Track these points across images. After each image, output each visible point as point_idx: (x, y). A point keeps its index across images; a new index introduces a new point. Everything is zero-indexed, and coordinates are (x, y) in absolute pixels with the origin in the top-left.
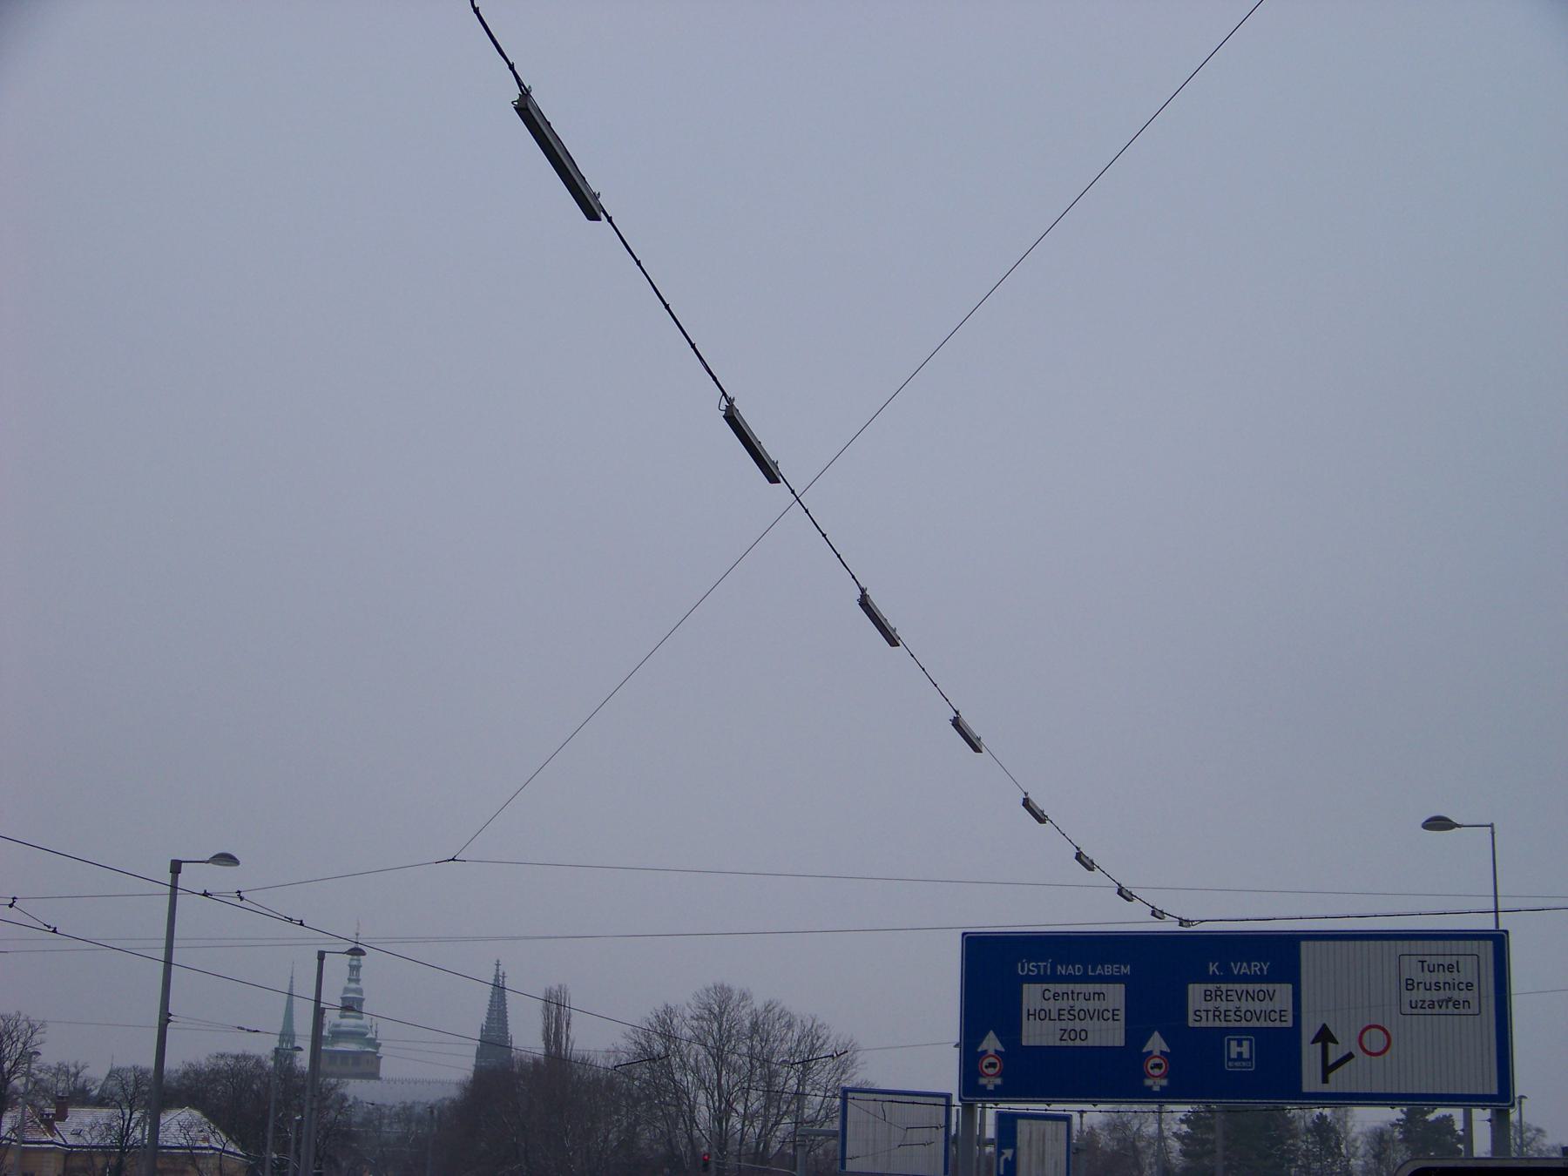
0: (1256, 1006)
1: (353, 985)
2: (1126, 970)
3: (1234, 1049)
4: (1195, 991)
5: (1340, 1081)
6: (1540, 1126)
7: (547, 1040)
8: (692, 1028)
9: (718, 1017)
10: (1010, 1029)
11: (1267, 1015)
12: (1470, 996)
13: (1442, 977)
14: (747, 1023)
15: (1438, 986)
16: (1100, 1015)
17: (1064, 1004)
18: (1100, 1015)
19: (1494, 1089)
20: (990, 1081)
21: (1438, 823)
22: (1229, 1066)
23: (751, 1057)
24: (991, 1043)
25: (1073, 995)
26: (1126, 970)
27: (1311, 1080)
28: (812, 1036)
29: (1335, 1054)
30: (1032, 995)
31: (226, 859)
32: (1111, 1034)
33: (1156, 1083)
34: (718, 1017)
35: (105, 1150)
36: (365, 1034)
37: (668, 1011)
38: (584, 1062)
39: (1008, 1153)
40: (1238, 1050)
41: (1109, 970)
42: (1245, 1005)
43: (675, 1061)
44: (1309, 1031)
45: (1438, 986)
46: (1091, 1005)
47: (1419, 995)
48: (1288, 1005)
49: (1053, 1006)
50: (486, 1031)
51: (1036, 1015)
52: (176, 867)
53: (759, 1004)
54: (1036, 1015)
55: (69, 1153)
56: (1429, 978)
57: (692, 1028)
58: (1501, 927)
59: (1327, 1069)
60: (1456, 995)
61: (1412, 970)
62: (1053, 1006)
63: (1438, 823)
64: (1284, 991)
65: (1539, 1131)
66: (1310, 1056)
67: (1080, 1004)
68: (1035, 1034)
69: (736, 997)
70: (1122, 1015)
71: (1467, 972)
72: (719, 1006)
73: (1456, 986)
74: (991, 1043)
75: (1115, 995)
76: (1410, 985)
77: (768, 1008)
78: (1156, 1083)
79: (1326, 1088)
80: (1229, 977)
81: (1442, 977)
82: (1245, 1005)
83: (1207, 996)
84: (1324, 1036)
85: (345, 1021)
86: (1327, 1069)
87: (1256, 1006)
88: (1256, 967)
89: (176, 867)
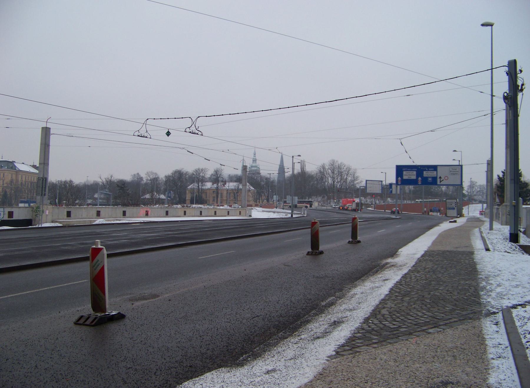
0: (432, 174)
1: (255, 157)
2: (416, 170)
3: (429, 179)
4: (425, 172)
5: (442, 183)
6: (477, 181)
7: (301, 169)
8: (328, 167)
9: (333, 165)
10: (402, 177)
11: (433, 175)
12: (458, 173)
13: (454, 170)
14: (337, 166)
15: (454, 172)
16: (413, 175)
17: (409, 174)
18: (413, 175)
19: (460, 184)
20: (399, 183)
21: (455, 151)
22: (428, 181)
23: (338, 172)
24: (399, 179)
25: (409, 173)
26: (416, 170)
27: (438, 183)
28: (349, 169)
29: (441, 180)
30: (404, 173)
31: (299, 156)
32: (414, 177)
33: (420, 183)
34: (333, 165)
35: (235, 189)
36: (257, 166)
37: (324, 164)
38: (307, 172)
39: (391, 189)
40: (430, 179)
41: (414, 170)
42: (431, 174)
43: (325, 173)
44: (438, 177)
45: (454, 172)
46: (412, 174)
47: (452, 172)
48: (436, 174)
49: (407, 174)
50: (280, 165)
51: (405, 175)
52: (293, 157)
53: (339, 162)
54: (405, 175)
55: (227, 190)
56: (453, 170)
57: (328, 167)
58: (506, 64)
59: (440, 181)
60: (456, 173)
61: (451, 169)
62: (407, 174)
63: (455, 151)
64: (435, 172)
65: (476, 182)
66: (438, 180)
67: (410, 174)
68: (405, 177)
69: (336, 162)
70: (415, 175)
71: (457, 170)
72: (333, 163)
73: (456, 172)
74: (399, 179)
75: (415, 173)
76: (451, 171)
77: (341, 163)
78: (420, 183)
79: (440, 184)
80: (429, 170)
81: (454, 170)
82: (431, 174)
83: (426, 173)
84: (440, 178)
85: (253, 164)
86: (440, 181)
87: (432, 174)
88: (432, 169)
89: (293, 157)
